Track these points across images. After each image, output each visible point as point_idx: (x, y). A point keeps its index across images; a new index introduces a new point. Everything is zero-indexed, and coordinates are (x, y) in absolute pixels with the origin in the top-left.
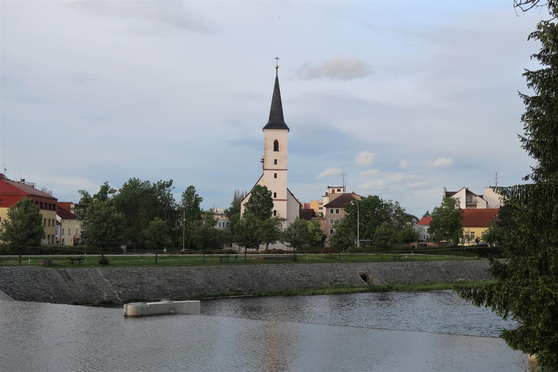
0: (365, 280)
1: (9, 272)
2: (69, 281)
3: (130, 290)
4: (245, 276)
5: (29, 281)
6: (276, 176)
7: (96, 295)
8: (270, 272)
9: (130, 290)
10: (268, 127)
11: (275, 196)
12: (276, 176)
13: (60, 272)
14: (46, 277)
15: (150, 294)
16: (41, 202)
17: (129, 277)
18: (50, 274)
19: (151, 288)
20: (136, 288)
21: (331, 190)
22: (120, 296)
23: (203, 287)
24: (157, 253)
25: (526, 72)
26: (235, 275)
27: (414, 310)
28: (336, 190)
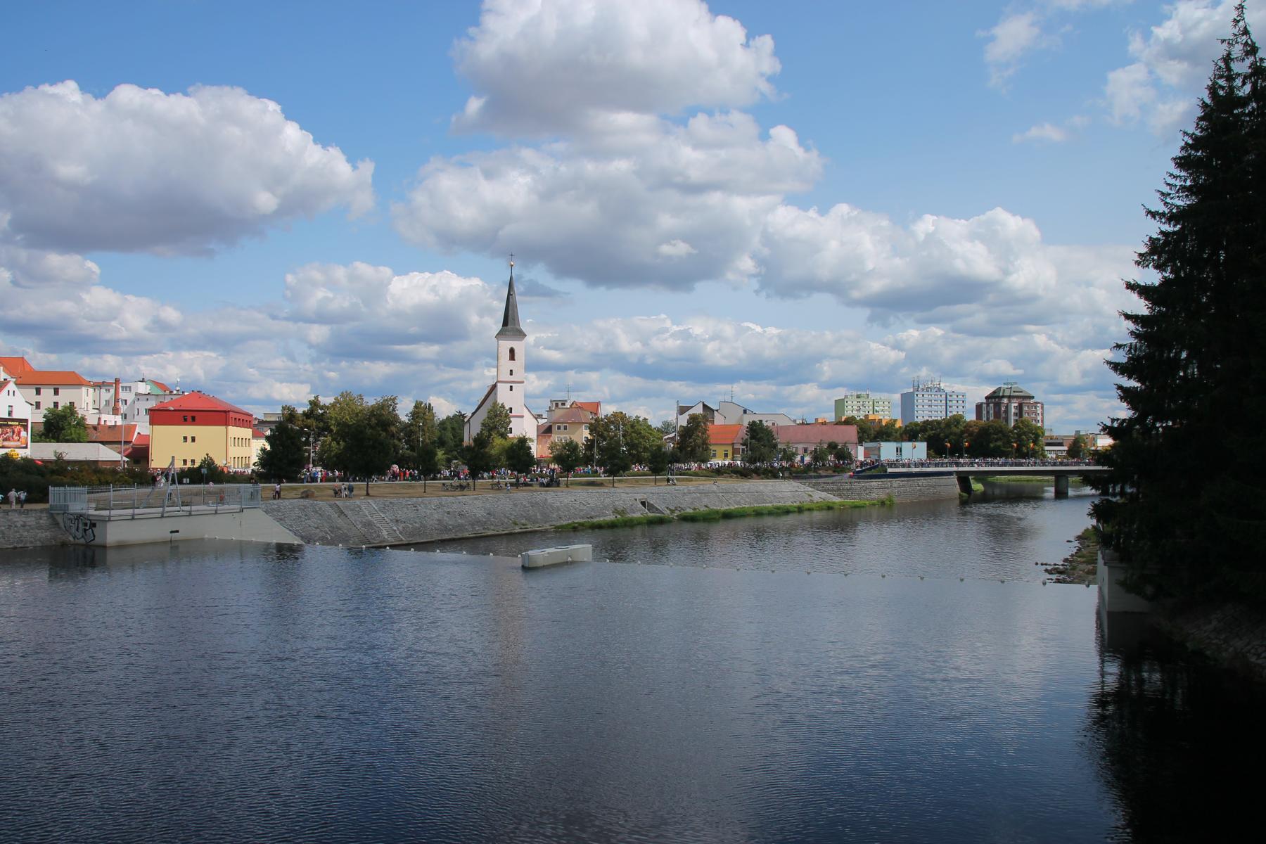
0: (644, 506)
1: (276, 506)
2: (342, 516)
3: (410, 526)
4: (525, 506)
5: (300, 517)
6: (511, 388)
7: (375, 532)
8: (549, 501)
9: (410, 526)
10: (500, 335)
11: (511, 412)
12: (511, 388)
13: (331, 506)
14: (316, 512)
15: (432, 530)
16: (196, 418)
17: (405, 510)
18: (320, 509)
19: (431, 523)
20: (416, 523)
21: (554, 403)
22: (401, 533)
23: (484, 520)
24: (656, 476)
25: (1115, 345)
26: (515, 505)
27: (245, 577)
28: (560, 404)
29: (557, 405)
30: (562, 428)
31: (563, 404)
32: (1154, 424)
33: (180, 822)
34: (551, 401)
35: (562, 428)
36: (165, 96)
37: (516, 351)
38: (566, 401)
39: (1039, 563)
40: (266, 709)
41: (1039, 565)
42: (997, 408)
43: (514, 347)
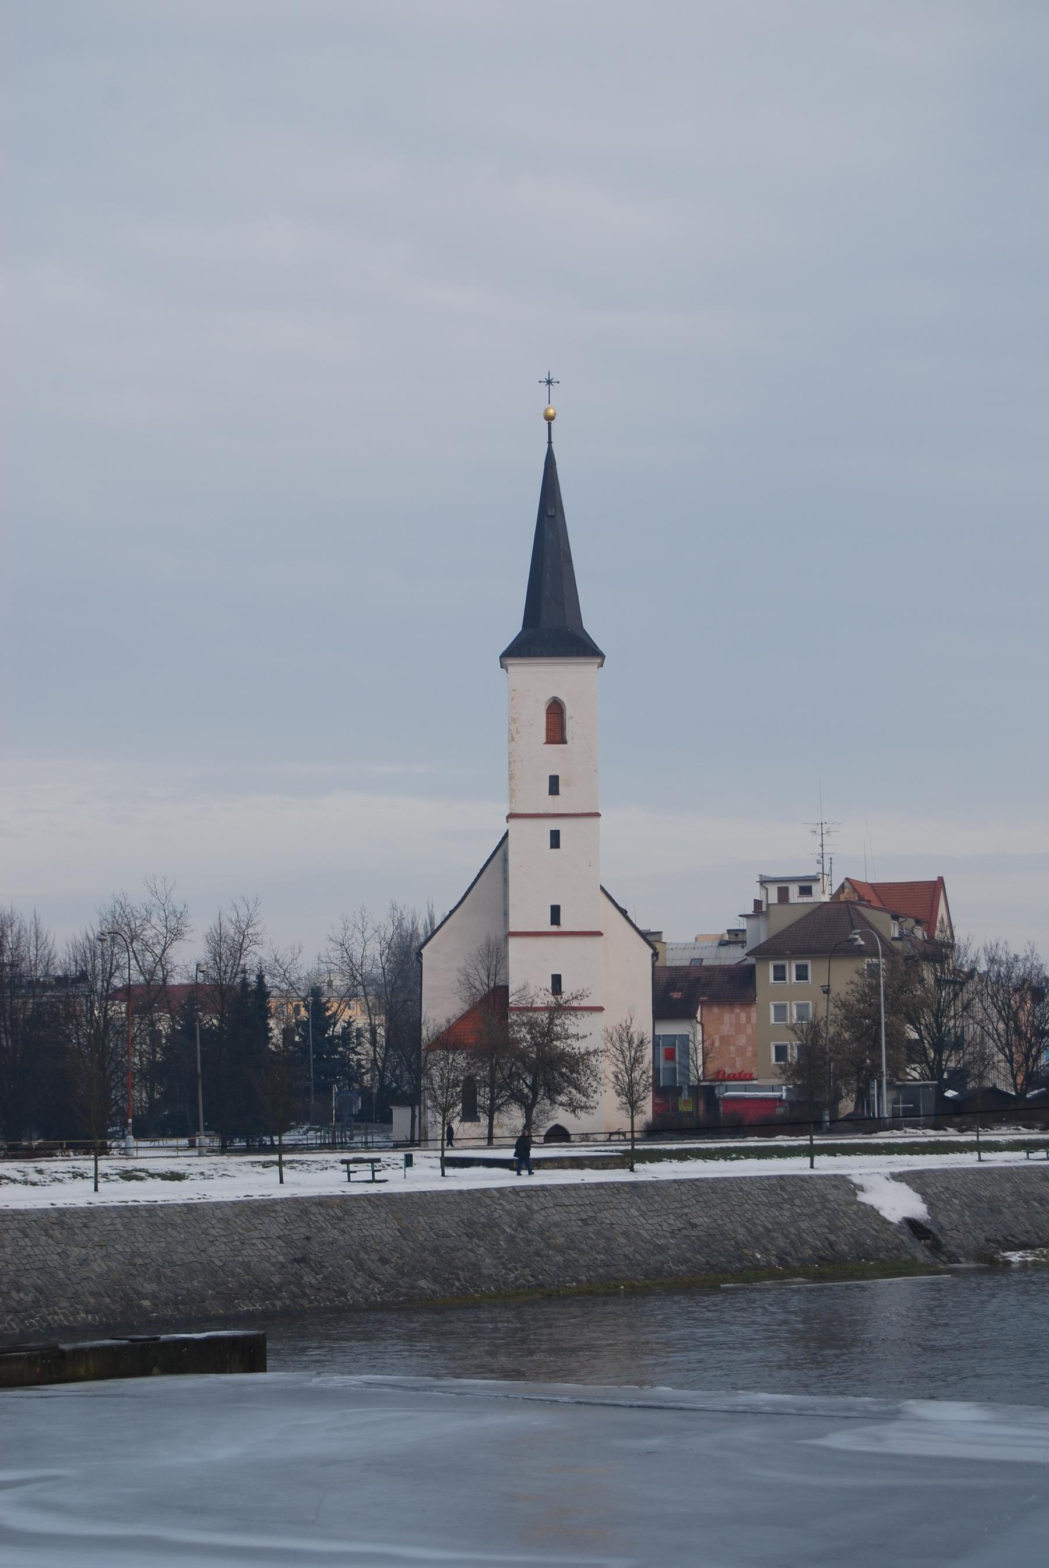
6: (555, 839)
12: (555, 839)
28: (794, 890)
29: (783, 894)
30: (791, 972)
31: (806, 891)
32: (90, 1030)
33: (669, 1350)
34: (764, 882)
35: (791, 972)
36: (560, 778)
37: (569, 712)
38: (816, 879)
39: (589, 1037)
40: (933, 1349)
41: (588, 1034)
42: (457, 1162)
43: (563, 698)
